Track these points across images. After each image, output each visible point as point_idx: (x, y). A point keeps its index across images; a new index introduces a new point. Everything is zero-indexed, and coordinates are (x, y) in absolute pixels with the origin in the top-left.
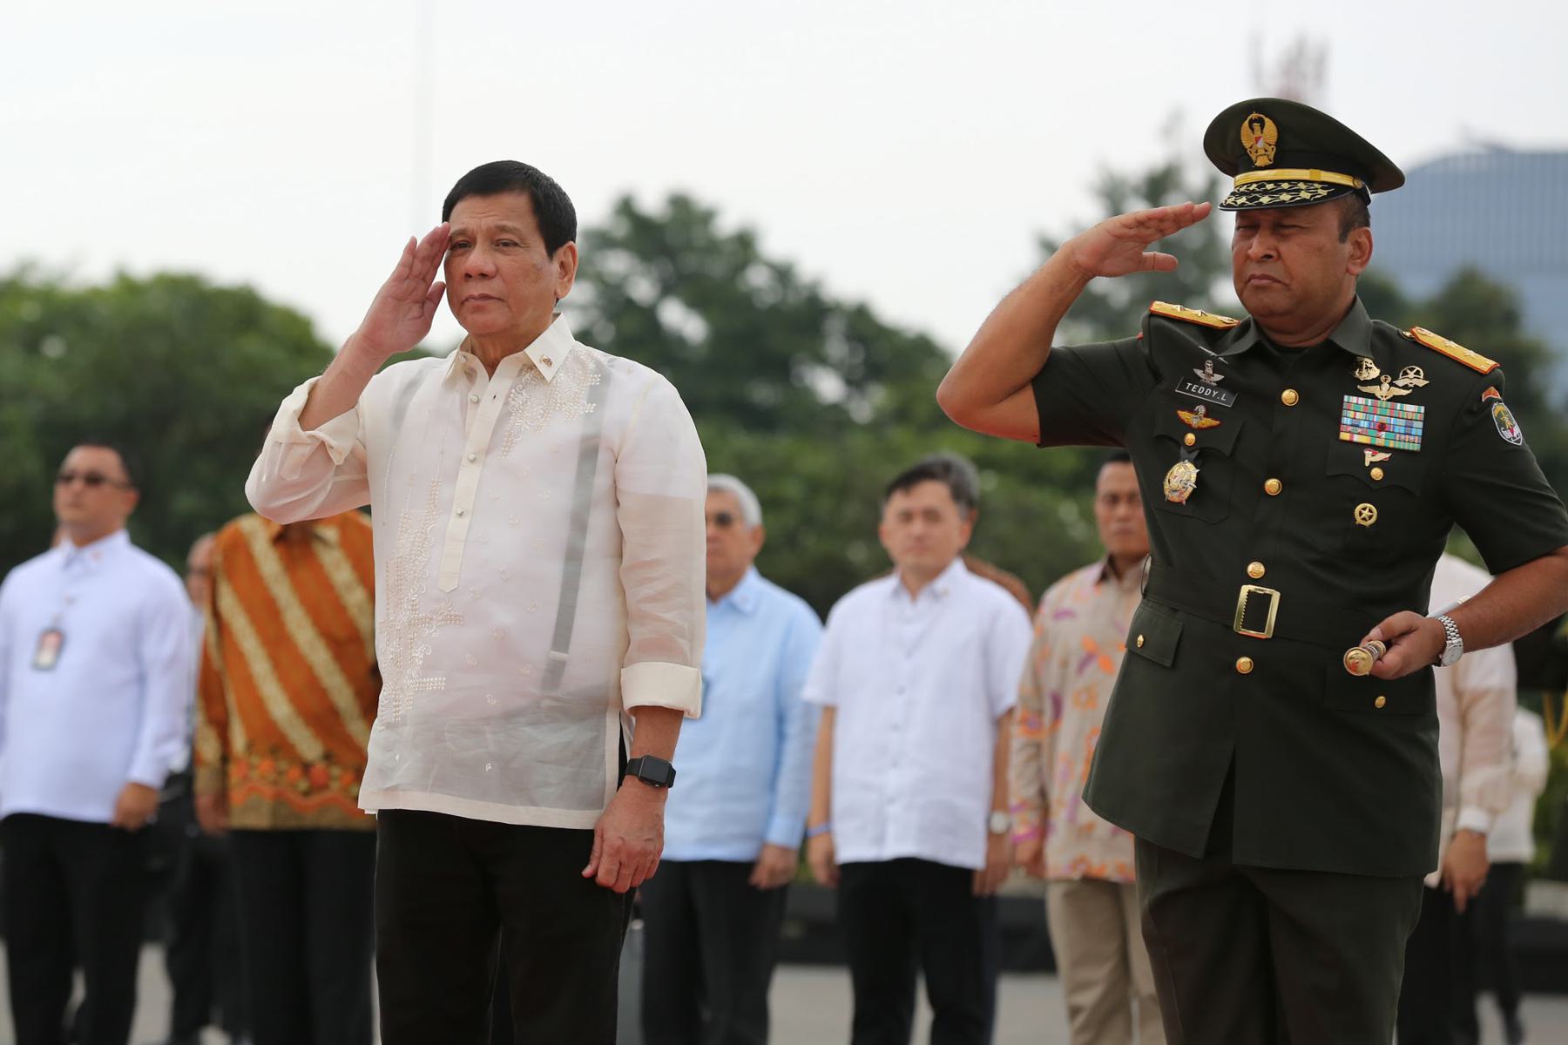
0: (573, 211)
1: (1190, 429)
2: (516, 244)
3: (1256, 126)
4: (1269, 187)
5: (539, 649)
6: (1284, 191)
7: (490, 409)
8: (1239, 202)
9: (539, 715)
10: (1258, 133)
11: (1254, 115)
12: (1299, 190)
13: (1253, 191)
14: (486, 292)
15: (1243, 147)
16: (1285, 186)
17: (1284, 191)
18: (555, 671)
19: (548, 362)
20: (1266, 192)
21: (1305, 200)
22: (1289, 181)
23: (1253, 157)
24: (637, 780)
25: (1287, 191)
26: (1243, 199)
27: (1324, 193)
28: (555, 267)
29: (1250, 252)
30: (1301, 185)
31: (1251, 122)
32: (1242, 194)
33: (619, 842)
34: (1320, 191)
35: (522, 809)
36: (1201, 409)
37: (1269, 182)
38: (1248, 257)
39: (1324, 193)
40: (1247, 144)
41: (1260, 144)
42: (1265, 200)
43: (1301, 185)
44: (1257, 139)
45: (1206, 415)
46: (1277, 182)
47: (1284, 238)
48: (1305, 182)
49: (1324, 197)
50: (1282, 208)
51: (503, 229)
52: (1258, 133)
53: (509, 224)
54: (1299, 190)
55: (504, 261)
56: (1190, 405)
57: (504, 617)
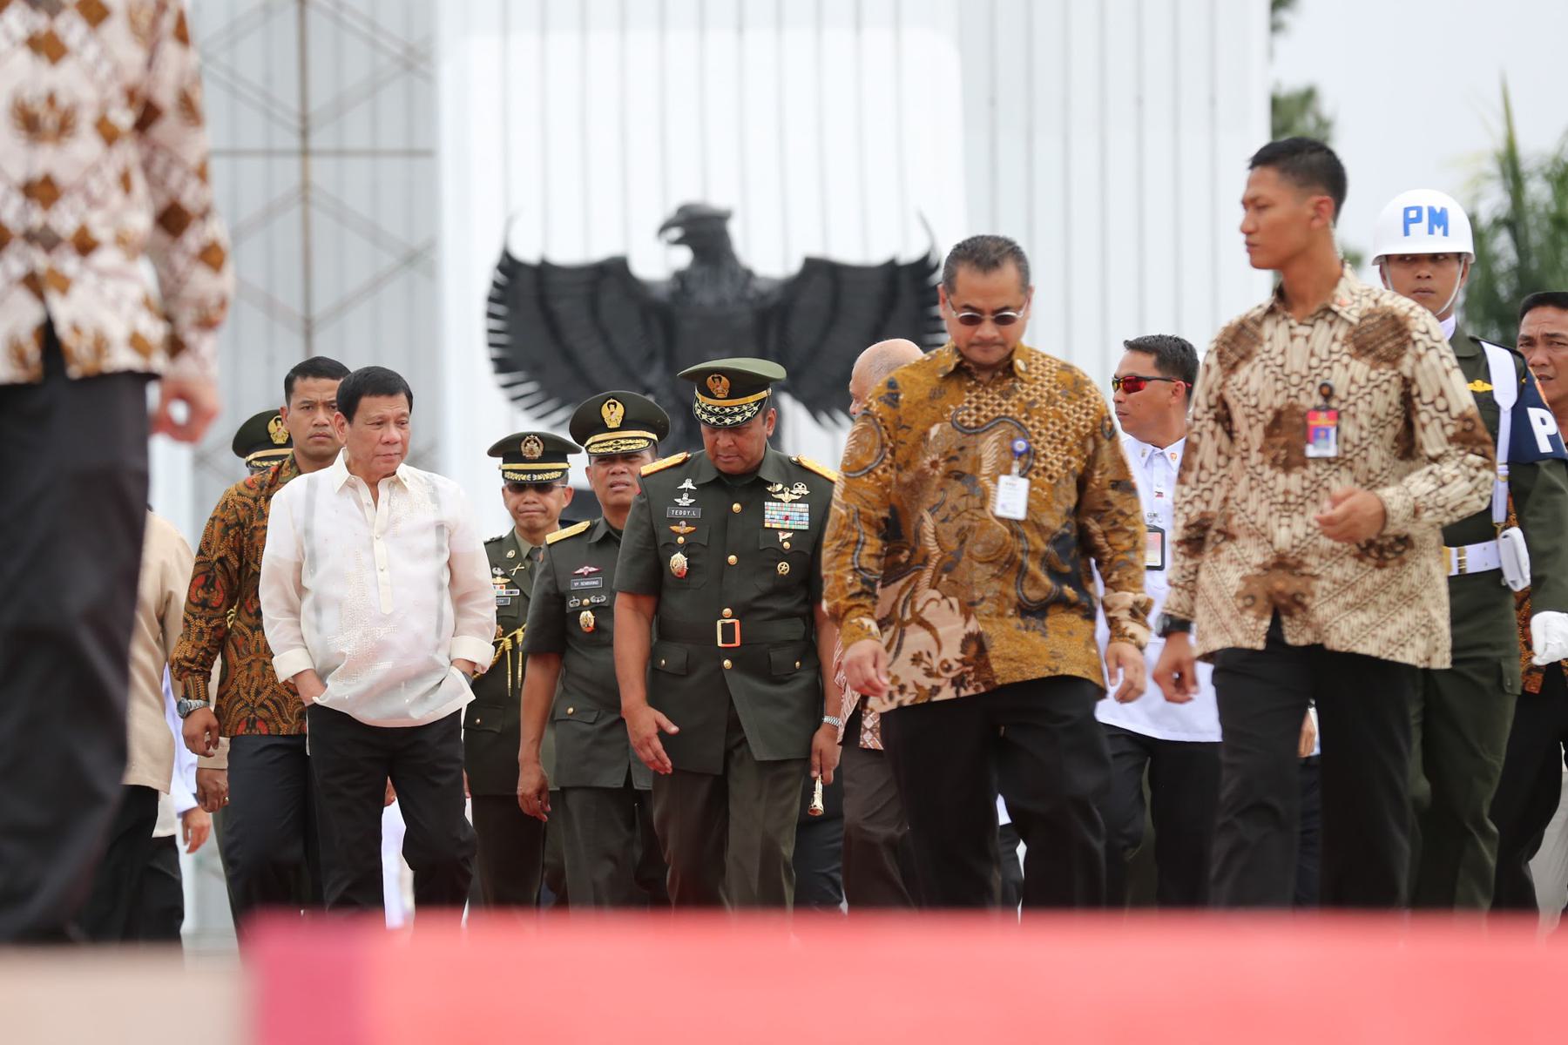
1: (679, 534)
11: (612, 401)
31: (609, 404)
36: (683, 523)
56: (676, 521)
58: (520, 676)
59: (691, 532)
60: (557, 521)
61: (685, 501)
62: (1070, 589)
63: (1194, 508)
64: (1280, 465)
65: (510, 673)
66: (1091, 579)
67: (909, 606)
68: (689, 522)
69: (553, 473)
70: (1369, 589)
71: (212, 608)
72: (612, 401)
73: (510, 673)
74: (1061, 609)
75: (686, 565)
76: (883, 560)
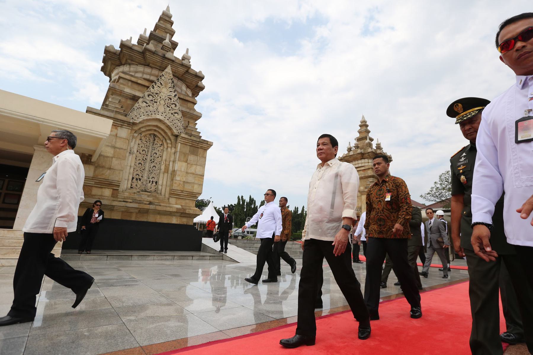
0: (336, 140)
1: (461, 170)
2: (326, 145)
3: (457, 106)
4: (465, 116)
5: (328, 209)
6: (468, 115)
7: (322, 172)
8: (459, 121)
9: (331, 221)
10: (458, 107)
11: (456, 104)
12: (472, 114)
13: (462, 118)
14: (321, 152)
15: (456, 111)
16: (468, 114)
17: (468, 115)
18: (331, 213)
19: (332, 164)
20: (464, 117)
21: (474, 115)
22: (468, 113)
23: (458, 112)
24: (344, 229)
25: (469, 115)
26: (460, 120)
27: (477, 112)
28: (334, 149)
29: (466, 129)
30: (471, 113)
31: (455, 106)
32: (459, 120)
33: (339, 240)
34: (476, 112)
35: (325, 238)
36: (462, 166)
37: (464, 115)
38: (465, 130)
39: (477, 112)
40: (456, 110)
41: (459, 109)
42: (465, 118)
43: (471, 113)
44: (458, 108)
45: (463, 166)
46: (466, 114)
47: (473, 123)
48: (472, 112)
49: (477, 113)
50: (469, 118)
51: (324, 142)
52: (458, 107)
53: (325, 141)
54: (472, 114)
55: (325, 147)
56: (459, 166)
57: (321, 204)
58: (115, 280)
59: (464, 168)
60: (38, 322)
61: (463, 159)
62: (383, 266)
63: (68, 205)
64: (59, 233)
65: (352, 257)
66: (120, 269)
67: (430, 262)
68: (463, 165)
69: (277, 229)
70: (65, 326)
71: (383, 225)
72: (456, 104)
73: (352, 257)
74: (77, 251)
75: (465, 179)
76: (399, 194)
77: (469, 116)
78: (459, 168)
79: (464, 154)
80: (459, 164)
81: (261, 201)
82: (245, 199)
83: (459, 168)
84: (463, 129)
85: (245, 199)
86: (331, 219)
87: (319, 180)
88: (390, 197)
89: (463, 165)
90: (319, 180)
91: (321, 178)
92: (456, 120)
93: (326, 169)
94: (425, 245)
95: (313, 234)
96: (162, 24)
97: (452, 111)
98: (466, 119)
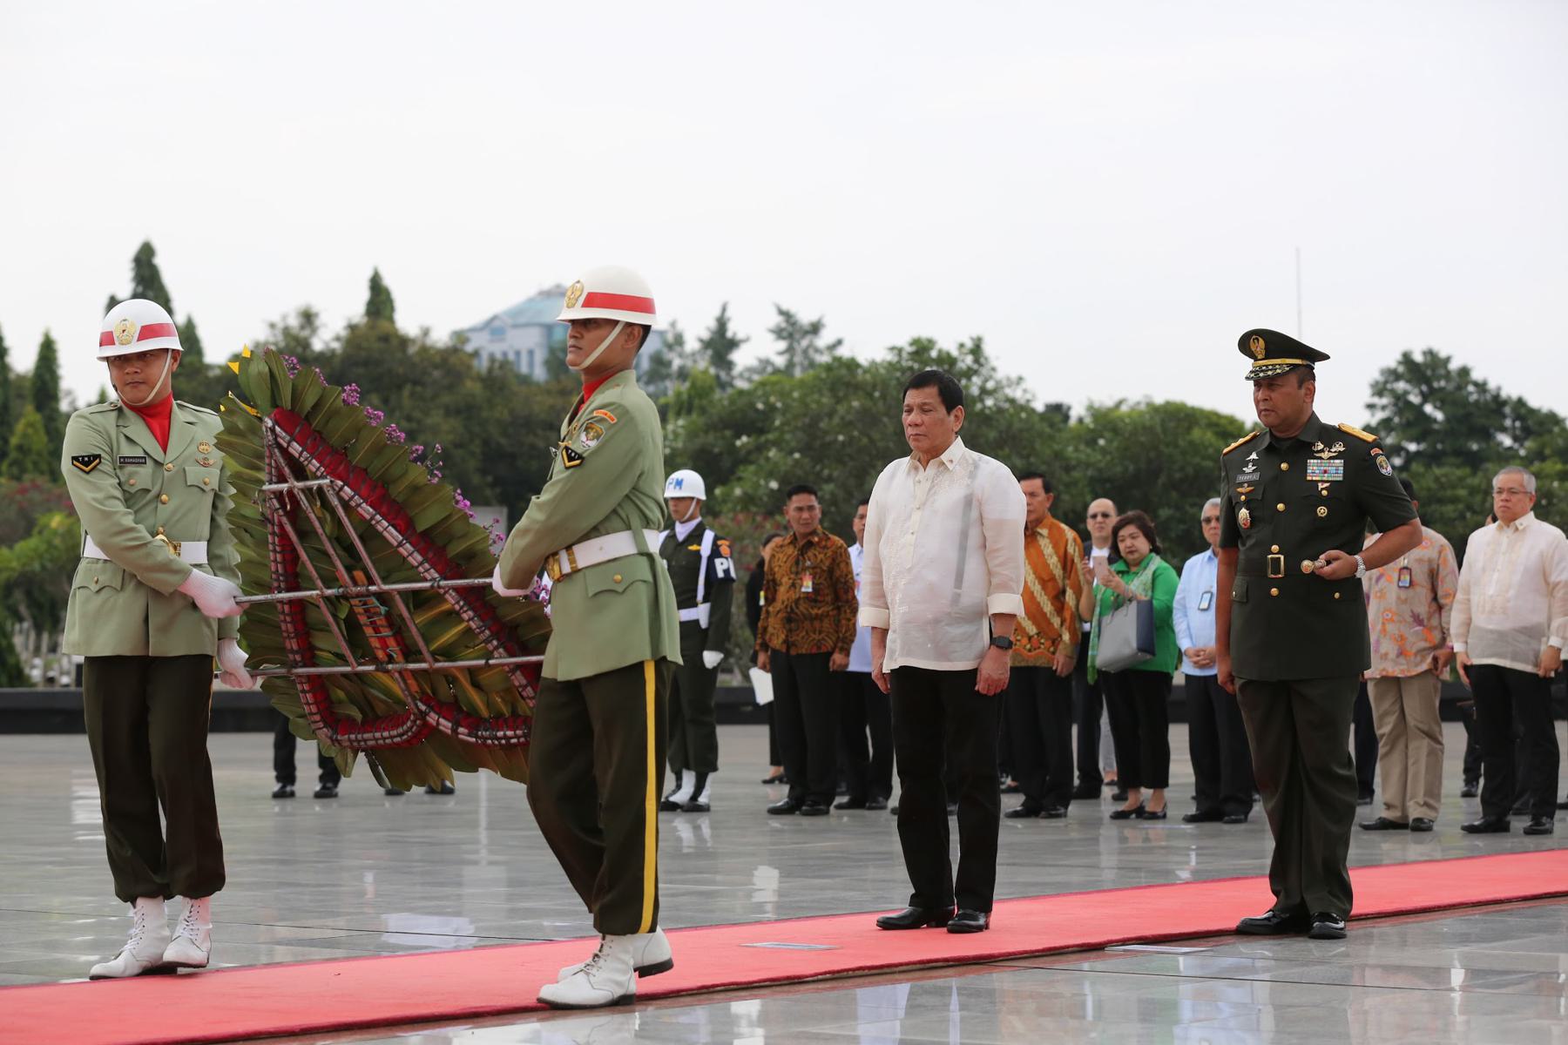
1: (1242, 494)
3: (1256, 341)
5: (948, 588)
18: (956, 598)
20: (1262, 371)
22: (1272, 365)
30: (1277, 366)
40: (1253, 350)
41: (1258, 349)
53: (926, 401)
56: (1241, 485)
57: (932, 576)
61: (1250, 468)
77: (1270, 373)
78: (1240, 490)
79: (1254, 456)
80: (1241, 478)
81: (285, 311)
82: (48, 352)
83: (1240, 490)
84: (1203, 422)
85: (48, 352)
86: (958, 615)
87: (919, 509)
88: (810, 584)
89: (1250, 483)
90: (919, 509)
91: (924, 504)
92: (1251, 369)
93: (937, 475)
94: (1349, 726)
95: (908, 653)
96: (636, 331)
97: (1245, 344)
98: (1264, 377)
